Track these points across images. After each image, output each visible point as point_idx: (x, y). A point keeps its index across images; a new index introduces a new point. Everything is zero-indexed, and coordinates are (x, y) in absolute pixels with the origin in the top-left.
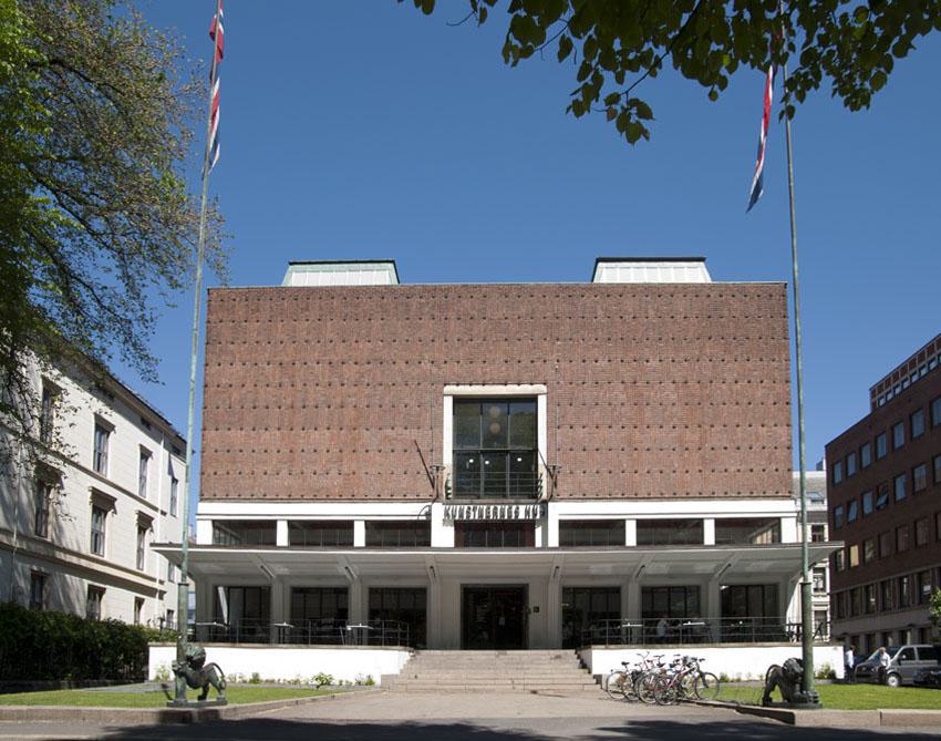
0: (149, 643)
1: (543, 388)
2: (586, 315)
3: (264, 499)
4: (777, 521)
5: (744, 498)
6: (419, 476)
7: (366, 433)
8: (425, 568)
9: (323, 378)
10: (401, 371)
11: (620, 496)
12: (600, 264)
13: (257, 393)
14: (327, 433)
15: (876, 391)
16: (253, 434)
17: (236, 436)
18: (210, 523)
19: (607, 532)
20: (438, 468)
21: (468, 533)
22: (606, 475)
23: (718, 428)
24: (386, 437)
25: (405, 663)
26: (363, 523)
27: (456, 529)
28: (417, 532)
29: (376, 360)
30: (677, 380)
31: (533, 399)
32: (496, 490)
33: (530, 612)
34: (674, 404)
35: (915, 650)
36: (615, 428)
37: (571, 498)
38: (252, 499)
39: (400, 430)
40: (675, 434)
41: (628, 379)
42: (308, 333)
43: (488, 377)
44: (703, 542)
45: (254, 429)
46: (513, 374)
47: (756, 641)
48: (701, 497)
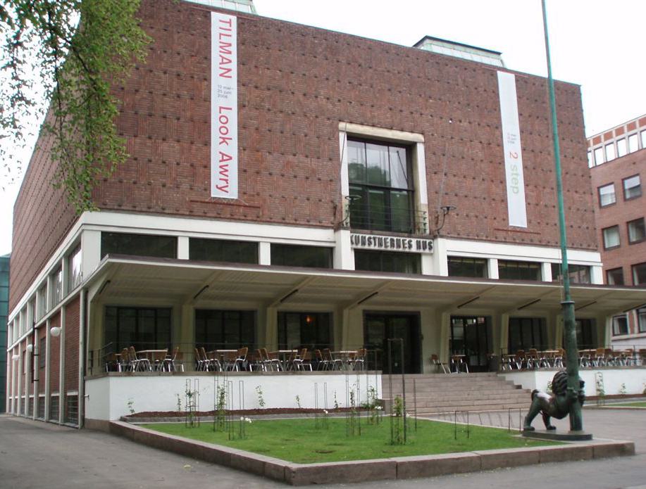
5: (461, 239)
6: (320, 203)
7: (270, 157)
9: (171, 89)
10: (299, 102)
11: (484, 238)
13: (153, 100)
14: (177, 146)
16: (149, 143)
19: (475, 267)
21: (365, 260)
22: (474, 219)
23: (548, 190)
24: (288, 163)
26: (550, 265)
28: (322, 257)
29: (276, 88)
30: (483, 141)
32: (388, 225)
35: (57, 395)
36: (477, 180)
39: (302, 158)
40: (483, 186)
43: (376, 121)
44: (176, 256)
45: (150, 138)
46: (397, 121)
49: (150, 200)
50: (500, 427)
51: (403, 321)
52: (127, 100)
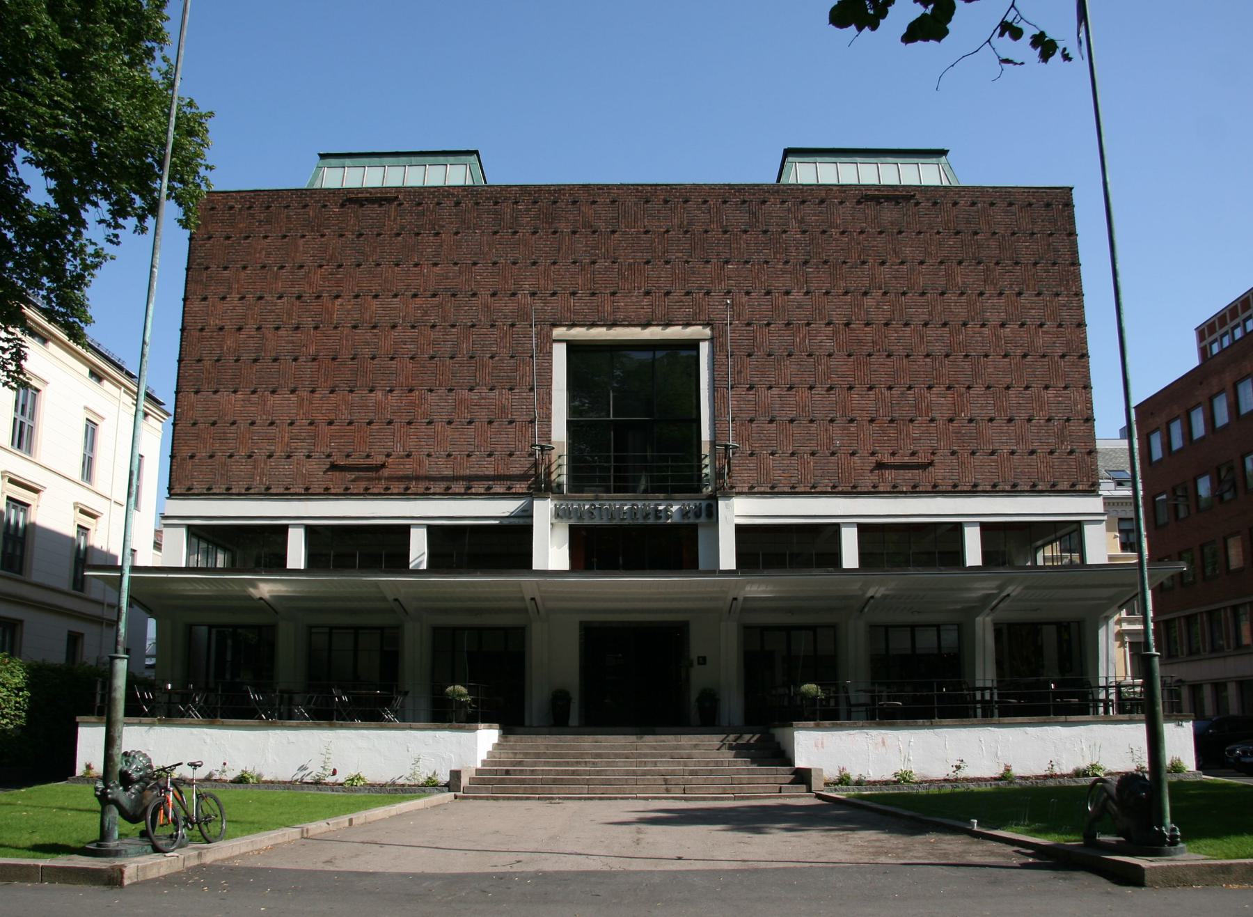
0: (78, 719)
1: (707, 332)
2: (771, 228)
3: (267, 494)
4: (1075, 526)
8: (523, 599)
12: (790, 159)
15: (1206, 332)
17: (231, 403)
18: (183, 531)
20: (542, 448)
23: (978, 390)
25: (490, 749)
27: (981, 530)
31: (694, 345)
33: (691, 665)
34: (830, 355)
37: (751, 493)
38: (247, 494)
41: (839, 320)
42: (268, 254)
43: (620, 315)
47: (1056, 714)
48: (954, 491)
49: (252, 478)
50: (897, 792)
51: (1053, 628)
52: (228, 342)
